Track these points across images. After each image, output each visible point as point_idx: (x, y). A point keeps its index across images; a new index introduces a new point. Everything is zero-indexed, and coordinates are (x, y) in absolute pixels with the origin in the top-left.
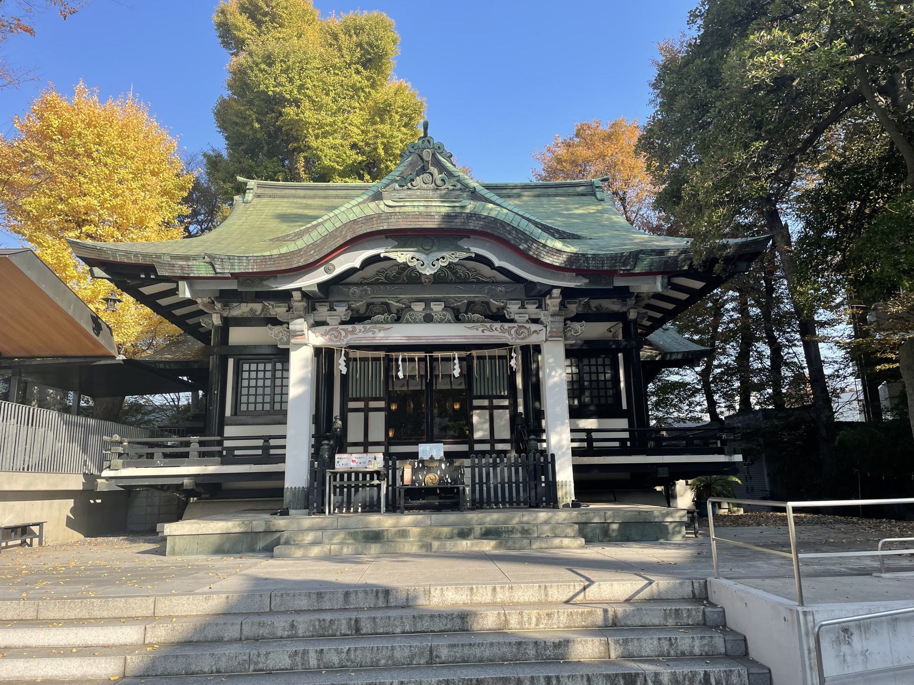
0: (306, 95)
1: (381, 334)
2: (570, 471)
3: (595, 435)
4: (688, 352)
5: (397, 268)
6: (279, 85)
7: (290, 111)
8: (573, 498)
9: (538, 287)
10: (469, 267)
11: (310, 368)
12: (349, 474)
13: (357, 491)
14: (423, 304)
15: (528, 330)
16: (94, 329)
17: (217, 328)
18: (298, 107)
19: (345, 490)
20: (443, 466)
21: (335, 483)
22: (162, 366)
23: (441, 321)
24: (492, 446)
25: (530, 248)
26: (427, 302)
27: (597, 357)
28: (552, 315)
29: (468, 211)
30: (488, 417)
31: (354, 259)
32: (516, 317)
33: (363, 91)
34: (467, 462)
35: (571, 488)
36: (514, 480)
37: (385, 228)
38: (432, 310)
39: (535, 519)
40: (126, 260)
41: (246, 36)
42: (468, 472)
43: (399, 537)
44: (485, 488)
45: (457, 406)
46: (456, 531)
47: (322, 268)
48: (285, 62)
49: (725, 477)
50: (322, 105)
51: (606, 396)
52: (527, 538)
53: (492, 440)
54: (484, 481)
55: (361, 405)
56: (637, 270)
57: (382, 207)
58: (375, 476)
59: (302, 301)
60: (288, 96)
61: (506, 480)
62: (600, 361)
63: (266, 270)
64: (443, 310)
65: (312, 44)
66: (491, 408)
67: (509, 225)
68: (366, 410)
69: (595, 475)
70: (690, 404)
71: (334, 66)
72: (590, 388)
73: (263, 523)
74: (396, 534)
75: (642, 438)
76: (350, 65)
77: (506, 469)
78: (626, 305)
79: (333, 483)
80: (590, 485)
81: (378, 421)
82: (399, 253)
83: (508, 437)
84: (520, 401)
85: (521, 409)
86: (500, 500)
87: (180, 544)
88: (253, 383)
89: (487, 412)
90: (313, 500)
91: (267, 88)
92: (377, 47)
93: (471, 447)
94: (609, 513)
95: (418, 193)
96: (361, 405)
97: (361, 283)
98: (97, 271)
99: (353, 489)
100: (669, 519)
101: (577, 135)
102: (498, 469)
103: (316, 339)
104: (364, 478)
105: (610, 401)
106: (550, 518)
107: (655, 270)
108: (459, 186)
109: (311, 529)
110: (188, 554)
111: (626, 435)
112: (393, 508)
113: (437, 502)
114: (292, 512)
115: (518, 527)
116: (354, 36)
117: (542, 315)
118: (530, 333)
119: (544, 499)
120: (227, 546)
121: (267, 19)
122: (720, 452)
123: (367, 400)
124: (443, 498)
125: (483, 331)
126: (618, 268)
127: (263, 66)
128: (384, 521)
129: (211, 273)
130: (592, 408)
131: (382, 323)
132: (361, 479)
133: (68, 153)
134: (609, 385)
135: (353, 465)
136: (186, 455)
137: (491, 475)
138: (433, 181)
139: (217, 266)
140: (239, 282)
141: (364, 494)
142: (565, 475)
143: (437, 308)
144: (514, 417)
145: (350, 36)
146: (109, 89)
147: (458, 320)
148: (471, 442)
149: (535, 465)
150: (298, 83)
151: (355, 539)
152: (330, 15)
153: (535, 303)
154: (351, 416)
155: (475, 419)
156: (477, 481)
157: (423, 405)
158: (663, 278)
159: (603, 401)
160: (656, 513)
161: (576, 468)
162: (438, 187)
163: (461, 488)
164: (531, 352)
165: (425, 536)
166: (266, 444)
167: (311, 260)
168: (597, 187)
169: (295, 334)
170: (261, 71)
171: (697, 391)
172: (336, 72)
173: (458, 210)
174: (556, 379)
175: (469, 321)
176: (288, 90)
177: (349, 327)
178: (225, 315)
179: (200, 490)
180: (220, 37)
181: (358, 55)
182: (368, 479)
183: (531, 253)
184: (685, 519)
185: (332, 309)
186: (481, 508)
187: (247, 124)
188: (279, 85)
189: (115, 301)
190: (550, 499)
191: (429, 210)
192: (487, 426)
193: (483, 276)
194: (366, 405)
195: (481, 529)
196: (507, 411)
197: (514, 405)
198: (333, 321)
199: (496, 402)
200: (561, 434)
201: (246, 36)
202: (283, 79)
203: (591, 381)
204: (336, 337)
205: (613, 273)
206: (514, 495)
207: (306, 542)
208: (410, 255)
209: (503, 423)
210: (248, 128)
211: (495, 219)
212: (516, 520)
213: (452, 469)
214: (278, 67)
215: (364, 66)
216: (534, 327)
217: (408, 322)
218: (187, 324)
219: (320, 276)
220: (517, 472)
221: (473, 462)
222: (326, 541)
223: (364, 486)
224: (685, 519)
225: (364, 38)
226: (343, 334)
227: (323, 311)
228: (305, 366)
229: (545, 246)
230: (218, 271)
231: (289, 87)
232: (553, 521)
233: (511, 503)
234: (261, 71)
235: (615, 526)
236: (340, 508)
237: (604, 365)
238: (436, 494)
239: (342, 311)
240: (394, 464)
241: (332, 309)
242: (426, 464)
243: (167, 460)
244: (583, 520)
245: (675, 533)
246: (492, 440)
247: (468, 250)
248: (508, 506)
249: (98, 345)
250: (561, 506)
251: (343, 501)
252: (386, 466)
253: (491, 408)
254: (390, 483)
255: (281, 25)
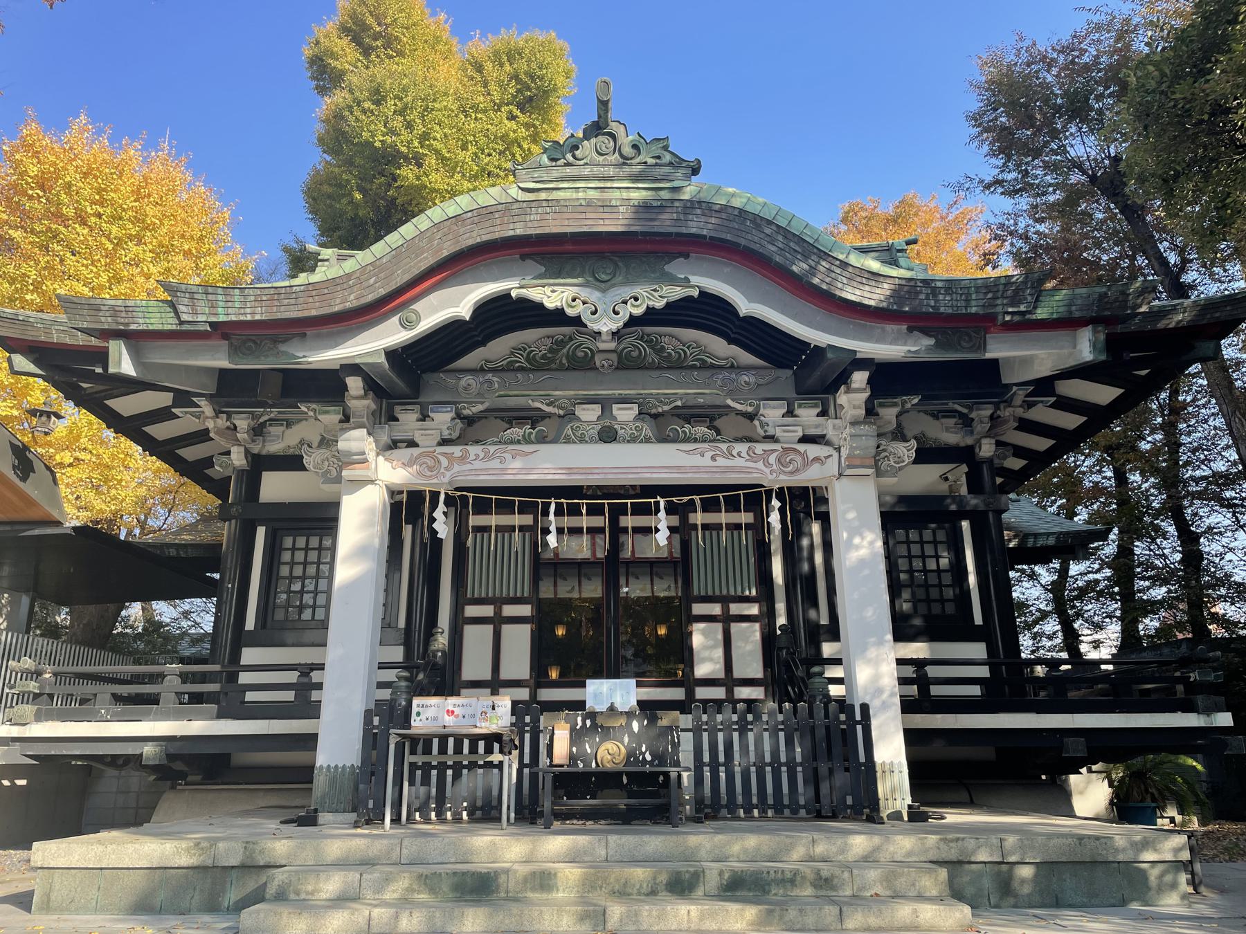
0: (430, 147)
1: (518, 464)
2: (899, 742)
3: (932, 671)
4: (1068, 533)
5: (549, 342)
6: (394, 132)
7: (407, 173)
8: (909, 801)
9: (830, 355)
10: (685, 339)
11: (377, 528)
12: (443, 739)
13: (457, 776)
14: (598, 408)
15: (804, 455)
16: (14, 467)
17: (241, 473)
18: (420, 166)
19: (434, 772)
20: (635, 726)
21: (413, 759)
22: (173, 552)
23: (633, 440)
24: (730, 692)
25: (813, 271)
26: (605, 404)
27: (921, 528)
28: (853, 424)
29: (686, 197)
30: (720, 636)
31: (458, 302)
32: (779, 432)
33: (520, 146)
34: (686, 720)
35: (902, 777)
36: (783, 759)
37: (518, 232)
38: (615, 419)
39: (843, 851)
40: (68, 341)
41: (347, 67)
42: (687, 740)
43: (533, 889)
44: (723, 775)
45: (662, 631)
46: (663, 878)
47: (395, 319)
48: (401, 99)
49: (1172, 757)
50: (457, 163)
51: (942, 601)
52: (832, 901)
53: (729, 680)
54: (722, 759)
55: (488, 611)
56: (1041, 314)
57: (514, 192)
58: (496, 746)
59: (365, 396)
60: (404, 149)
61: (768, 759)
62: (927, 535)
63: (279, 316)
64: (637, 418)
65: (448, 76)
66: (727, 620)
67: (770, 222)
68: (498, 621)
69: (938, 750)
70: (1035, 637)
71: (475, 108)
72: (911, 584)
73: (239, 847)
74: (525, 880)
75: (1009, 683)
76: (500, 106)
77: (766, 735)
78: (972, 433)
79: (409, 758)
80: (945, 772)
81: (518, 641)
82: (547, 290)
83: (759, 674)
84: (781, 607)
85: (781, 620)
86: (755, 800)
87: (62, 888)
88: (298, 571)
89: (718, 627)
90: (364, 797)
91: (373, 136)
92: (541, 78)
93: (690, 694)
94: (1011, 840)
95: (586, 171)
96: (488, 611)
97: (482, 370)
98: (21, 362)
99: (450, 772)
100: (1149, 856)
101: (845, 220)
102: (751, 735)
103: (393, 472)
104: (473, 750)
105: (950, 609)
106: (877, 849)
107: (1077, 314)
108: (667, 158)
109: (342, 864)
110: (77, 911)
111: (983, 672)
112: (530, 813)
113: (622, 803)
114: (324, 817)
115: (807, 870)
116: (507, 64)
117: (829, 427)
118: (808, 463)
119: (849, 800)
120: (160, 897)
121: (379, 43)
122: (1188, 707)
123: (498, 602)
124: (638, 796)
125: (713, 458)
126: (999, 309)
127: (367, 105)
128: (504, 849)
129: (170, 324)
130: (917, 622)
131: (519, 442)
132: (466, 750)
133: (49, 215)
134: (947, 579)
135: (449, 720)
136: (153, 700)
137: (736, 747)
138: (617, 149)
139: (181, 308)
140: (231, 345)
141: (473, 782)
142: (890, 749)
143: (625, 414)
144: (768, 641)
145: (501, 65)
146: (121, 122)
147: (663, 439)
148: (690, 683)
149: (828, 728)
150: (420, 129)
151: (432, 890)
152: (471, 38)
153: (816, 406)
154: (470, 631)
155: (697, 640)
156: (706, 759)
157: (606, 617)
158: (1095, 332)
159: (936, 609)
160: (1120, 842)
161: (912, 737)
162: (625, 160)
163: (673, 775)
164: (807, 504)
165: (593, 887)
166: (305, 680)
167: (370, 298)
168: (899, 251)
169: (347, 460)
170: (364, 111)
171: (1044, 615)
172: (479, 116)
173: (665, 195)
174: (863, 552)
175: (687, 440)
176: (403, 141)
177: (457, 450)
178: (256, 449)
179: (179, 766)
180: (313, 78)
181: (513, 91)
182: (481, 749)
183: (816, 281)
184: (1185, 855)
185: (424, 417)
186: (715, 818)
187: (344, 196)
188: (394, 132)
189: (49, 414)
190: (863, 806)
191: (606, 195)
192: (719, 653)
193: (712, 356)
194: (498, 612)
195: (721, 873)
196: (757, 626)
197: (771, 613)
198: (427, 437)
199: (735, 609)
200: (876, 663)
201: (347, 67)
202: (397, 123)
203: (911, 571)
204: (430, 469)
205: (984, 323)
206: (770, 789)
207: (324, 896)
208: (569, 292)
209: (749, 647)
210: (345, 201)
211: (741, 211)
212: (798, 852)
213: (654, 732)
214: (390, 106)
215: (521, 107)
216: (813, 450)
217: (568, 441)
218: (210, 479)
219: (391, 334)
220: (789, 743)
221: (697, 720)
222: (369, 895)
223: (473, 766)
224: (1185, 855)
225: (522, 66)
226: (444, 462)
227: (408, 419)
228: (368, 524)
229: (844, 265)
230: (185, 317)
231: (405, 135)
232: (883, 856)
233: (779, 808)
234: (364, 111)
235: (1026, 872)
236: (423, 809)
237: (935, 543)
238: (620, 786)
239: (443, 419)
240: (536, 721)
241: (424, 417)
242: (599, 721)
243: (120, 708)
244: (953, 855)
245: (1163, 888)
246: (729, 680)
247: (686, 283)
248: (770, 813)
249: (31, 503)
250: (884, 814)
251: (428, 797)
252: (518, 726)
253: (727, 620)
254: (527, 760)
255: (401, 54)
